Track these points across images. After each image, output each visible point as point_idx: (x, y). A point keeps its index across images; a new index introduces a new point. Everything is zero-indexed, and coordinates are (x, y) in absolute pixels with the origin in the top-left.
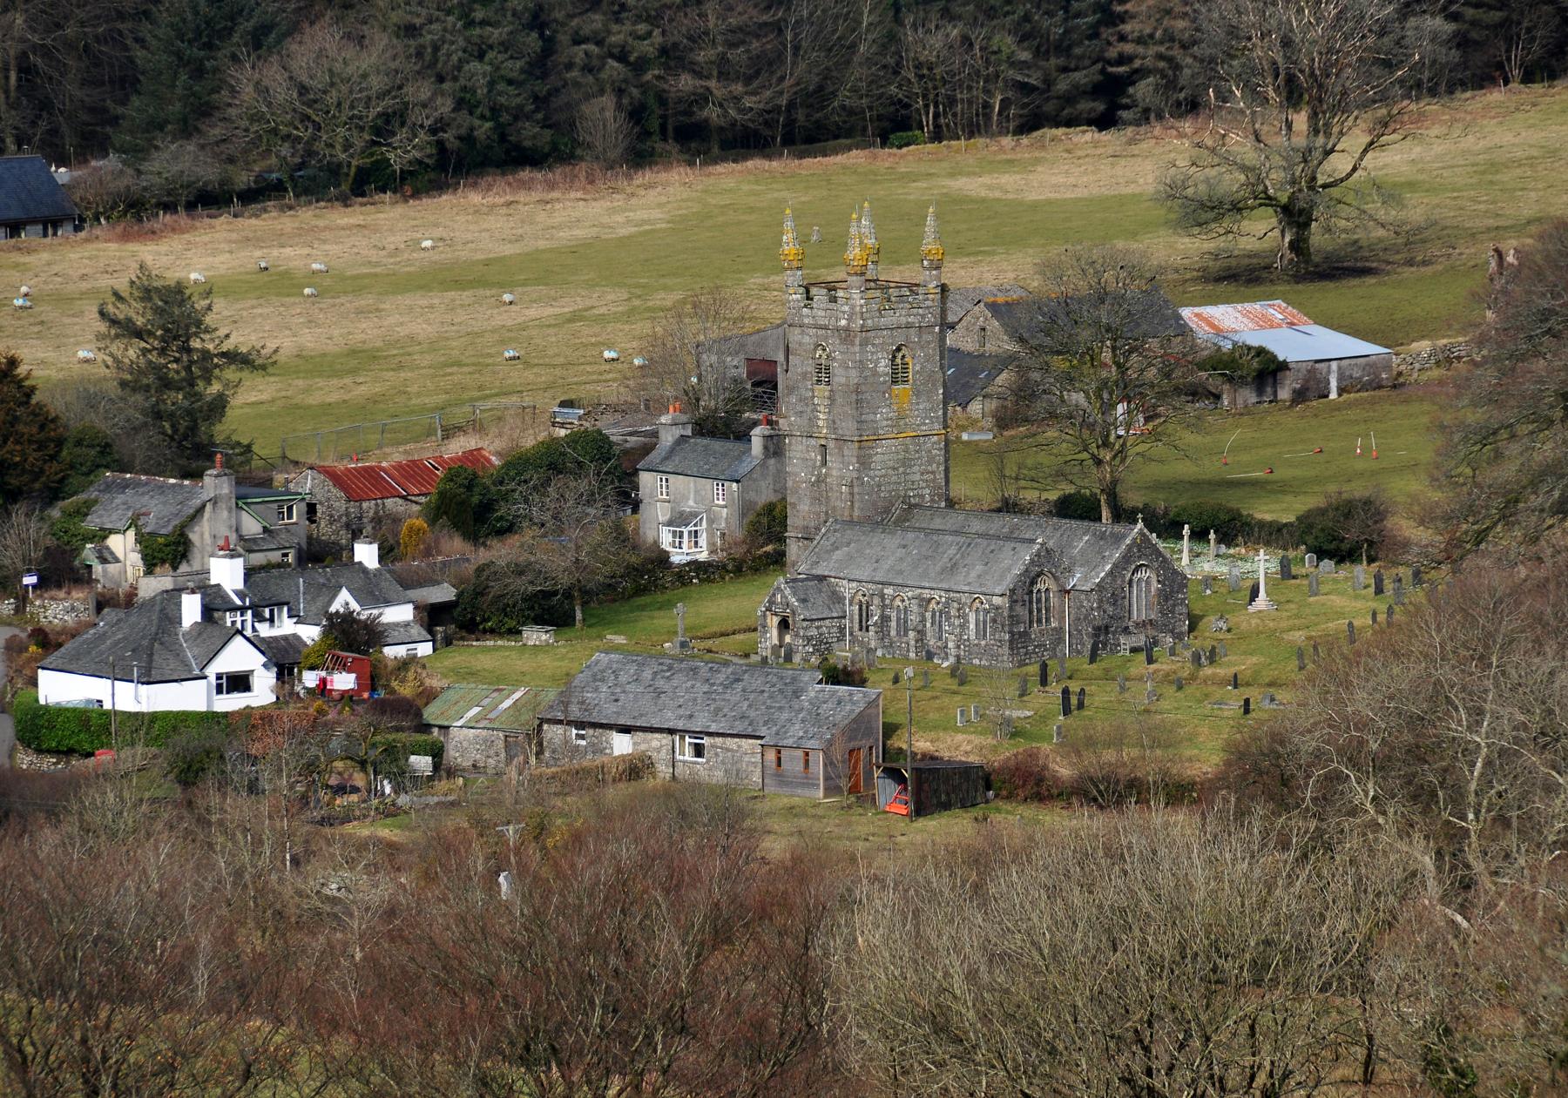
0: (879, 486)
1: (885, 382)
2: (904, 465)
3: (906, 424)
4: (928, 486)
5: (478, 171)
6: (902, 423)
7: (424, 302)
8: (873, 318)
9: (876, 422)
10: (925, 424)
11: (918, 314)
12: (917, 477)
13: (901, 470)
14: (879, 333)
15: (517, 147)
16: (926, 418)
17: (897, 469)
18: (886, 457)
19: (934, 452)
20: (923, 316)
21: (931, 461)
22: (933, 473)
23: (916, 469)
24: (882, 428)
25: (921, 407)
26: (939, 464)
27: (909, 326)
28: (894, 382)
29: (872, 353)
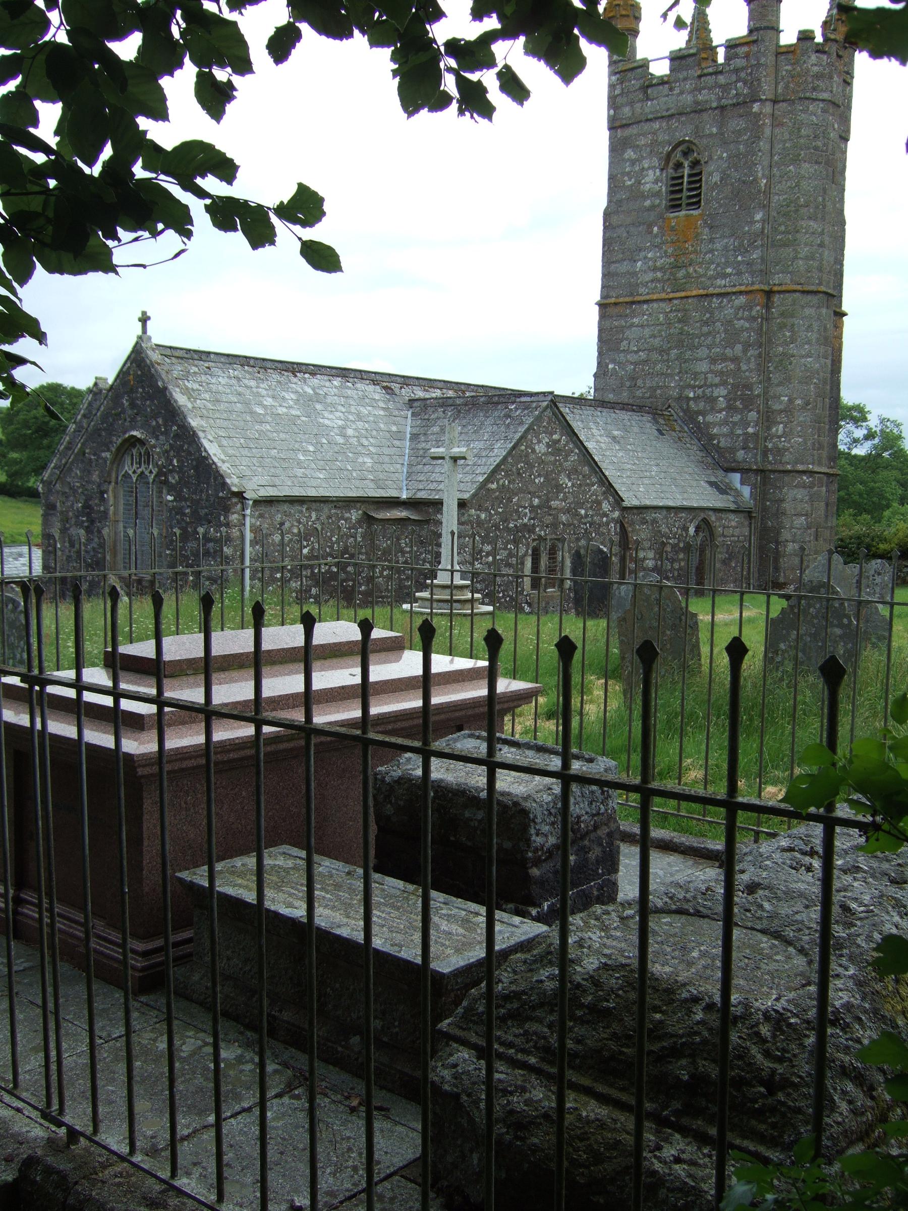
0: (633, 379)
1: (653, 207)
2: (680, 344)
3: (688, 276)
4: (724, 383)
5: (443, 784)
6: (681, 273)
7: (53, 1129)
8: (631, 104)
9: (634, 274)
10: (725, 276)
11: (717, 85)
12: (704, 367)
13: (674, 352)
14: (646, 127)
15: (787, 600)
16: (727, 264)
17: (667, 351)
18: (647, 332)
19: (739, 324)
20: (725, 88)
21: (732, 337)
22: (735, 360)
23: (703, 352)
24: (645, 285)
25: (718, 246)
26: (747, 346)
27: (699, 110)
28: (675, 206)
29: (633, 162)
